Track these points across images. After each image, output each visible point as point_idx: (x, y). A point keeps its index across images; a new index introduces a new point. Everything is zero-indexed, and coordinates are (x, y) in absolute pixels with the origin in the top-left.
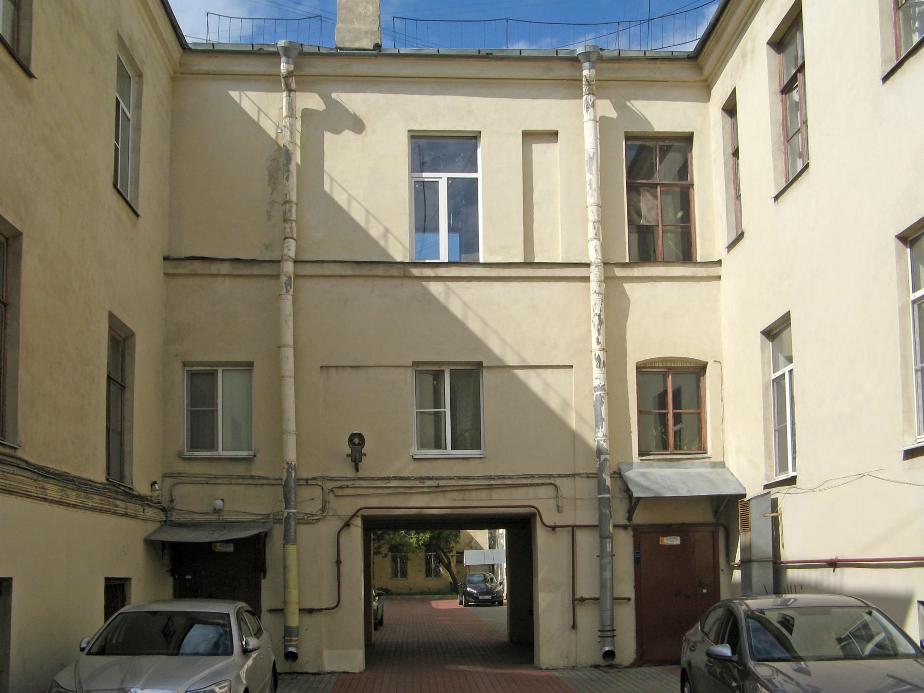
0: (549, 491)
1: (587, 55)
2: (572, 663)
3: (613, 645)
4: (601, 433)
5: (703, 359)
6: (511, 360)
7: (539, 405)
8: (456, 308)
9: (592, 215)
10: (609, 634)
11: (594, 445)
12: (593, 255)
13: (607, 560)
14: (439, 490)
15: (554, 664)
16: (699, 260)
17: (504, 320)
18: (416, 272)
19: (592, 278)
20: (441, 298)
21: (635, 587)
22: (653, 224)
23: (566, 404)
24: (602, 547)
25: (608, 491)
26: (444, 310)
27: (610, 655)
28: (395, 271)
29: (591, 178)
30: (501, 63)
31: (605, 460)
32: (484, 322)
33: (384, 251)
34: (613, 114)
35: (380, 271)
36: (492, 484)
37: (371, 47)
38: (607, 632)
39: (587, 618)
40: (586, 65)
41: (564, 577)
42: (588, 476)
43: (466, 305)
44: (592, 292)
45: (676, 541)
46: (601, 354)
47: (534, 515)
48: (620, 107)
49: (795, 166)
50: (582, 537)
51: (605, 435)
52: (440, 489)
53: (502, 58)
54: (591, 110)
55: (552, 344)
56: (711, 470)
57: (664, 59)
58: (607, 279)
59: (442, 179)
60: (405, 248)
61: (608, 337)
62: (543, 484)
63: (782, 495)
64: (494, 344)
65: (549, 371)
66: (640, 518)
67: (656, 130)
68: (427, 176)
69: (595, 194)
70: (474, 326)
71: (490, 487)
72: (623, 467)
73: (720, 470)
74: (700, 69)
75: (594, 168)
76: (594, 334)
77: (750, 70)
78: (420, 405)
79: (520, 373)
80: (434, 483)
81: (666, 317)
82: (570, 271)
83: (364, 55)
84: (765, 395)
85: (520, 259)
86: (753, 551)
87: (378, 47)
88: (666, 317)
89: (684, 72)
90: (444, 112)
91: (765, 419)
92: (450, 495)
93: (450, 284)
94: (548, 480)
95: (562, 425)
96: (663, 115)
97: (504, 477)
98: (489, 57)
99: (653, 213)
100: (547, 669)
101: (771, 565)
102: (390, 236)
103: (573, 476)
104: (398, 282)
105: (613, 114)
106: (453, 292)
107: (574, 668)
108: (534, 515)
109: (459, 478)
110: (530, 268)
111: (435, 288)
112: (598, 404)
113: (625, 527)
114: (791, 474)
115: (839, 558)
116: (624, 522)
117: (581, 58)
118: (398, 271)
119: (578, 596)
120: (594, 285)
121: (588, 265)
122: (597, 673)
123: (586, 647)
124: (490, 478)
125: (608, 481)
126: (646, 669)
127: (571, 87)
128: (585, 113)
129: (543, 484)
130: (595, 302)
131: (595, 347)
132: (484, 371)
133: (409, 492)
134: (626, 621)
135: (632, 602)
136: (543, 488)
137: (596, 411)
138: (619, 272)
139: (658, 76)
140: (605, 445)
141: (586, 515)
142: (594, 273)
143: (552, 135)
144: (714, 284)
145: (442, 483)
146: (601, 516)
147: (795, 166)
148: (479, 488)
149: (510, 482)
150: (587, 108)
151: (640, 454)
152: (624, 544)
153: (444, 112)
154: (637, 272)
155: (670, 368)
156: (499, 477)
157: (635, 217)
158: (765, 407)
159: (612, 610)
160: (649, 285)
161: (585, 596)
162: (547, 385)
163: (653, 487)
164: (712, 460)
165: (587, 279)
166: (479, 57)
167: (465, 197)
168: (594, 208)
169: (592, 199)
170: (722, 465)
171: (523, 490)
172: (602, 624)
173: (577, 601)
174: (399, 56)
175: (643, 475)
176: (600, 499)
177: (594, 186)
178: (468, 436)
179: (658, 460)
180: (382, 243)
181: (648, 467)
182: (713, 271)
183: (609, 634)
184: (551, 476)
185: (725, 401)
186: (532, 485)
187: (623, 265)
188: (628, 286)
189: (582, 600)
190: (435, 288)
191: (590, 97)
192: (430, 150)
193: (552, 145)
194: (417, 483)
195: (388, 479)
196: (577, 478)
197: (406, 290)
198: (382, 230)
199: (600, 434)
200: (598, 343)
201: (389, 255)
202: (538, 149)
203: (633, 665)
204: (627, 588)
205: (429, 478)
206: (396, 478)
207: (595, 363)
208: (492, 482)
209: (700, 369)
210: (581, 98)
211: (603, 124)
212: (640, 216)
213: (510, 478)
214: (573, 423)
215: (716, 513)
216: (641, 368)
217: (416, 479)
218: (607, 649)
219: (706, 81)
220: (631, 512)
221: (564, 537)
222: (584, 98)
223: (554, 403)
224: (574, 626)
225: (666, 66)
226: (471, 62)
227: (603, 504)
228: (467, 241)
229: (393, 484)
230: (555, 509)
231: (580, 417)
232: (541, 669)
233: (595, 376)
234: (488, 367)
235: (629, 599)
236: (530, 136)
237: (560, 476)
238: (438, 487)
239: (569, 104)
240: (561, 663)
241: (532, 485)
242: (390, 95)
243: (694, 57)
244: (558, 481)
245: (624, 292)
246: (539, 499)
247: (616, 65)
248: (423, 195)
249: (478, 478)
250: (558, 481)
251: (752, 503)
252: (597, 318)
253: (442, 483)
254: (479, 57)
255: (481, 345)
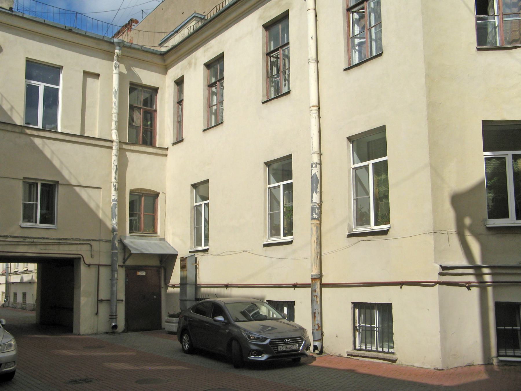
0: (87, 247)
1: (119, 44)
2: (95, 332)
3: (116, 322)
4: (115, 222)
5: (158, 191)
6: (73, 182)
7: (86, 205)
8: (48, 153)
9: (115, 118)
10: (115, 317)
11: (110, 227)
12: (114, 137)
13: (115, 282)
14: (33, 244)
15: (86, 332)
16: (157, 146)
17: (70, 162)
18: (28, 131)
19: (114, 148)
20: (40, 147)
21: (126, 295)
22: (139, 126)
23: (98, 206)
24: (113, 276)
25: (116, 249)
26: (41, 153)
27: (115, 327)
28: (17, 130)
29: (115, 100)
30: (76, 35)
31: (116, 234)
32: (61, 162)
33: (10, 118)
34: (125, 72)
35: (9, 128)
36: (61, 242)
37: (8, 9)
38: (113, 316)
39: (103, 309)
40: (118, 48)
41: (92, 289)
42: (106, 241)
43: (53, 152)
44: (113, 154)
45: (143, 273)
46: (116, 184)
47: (80, 258)
48: (128, 69)
49: (214, 118)
50: (103, 270)
51: (116, 223)
52: (34, 244)
53: (77, 34)
54: (117, 68)
55: (94, 177)
56: (159, 242)
57: (150, 52)
58: (121, 150)
59: (42, 86)
60: (21, 117)
61: (119, 176)
62: (85, 244)
63: (200, 257)
64: (66, 174)
65: (90, 189)
66: (129, 263)
67: (143, 83)
68: (34, 83)
69: (117, 108)
70: (56, 163)
71: (59, 244)
72: (122, 238)
73: (163, 242)
74: (164, 60)
75: (117, 96)
76: (113, 174)
77: (193, 72)
78: (24, 200)
79: (77, 189)
80: (32, 240)
81: (144, 170)
82: (103, 143)
83: (4, 12)
84: (191, 212)
85: (78, 133)
86: (188, 279)
87: (11, 9)
88: (144, 170)
89: (158, 60)
90: (46, 53)
91: (191, 222)
92: (39, 247)
93: (45, 140)
94: (88, 242)
95: (95, 215)
96: (147, 77)
97: (66, 239)
98: (70, 31)
99: (139, 121)
100: (83, 335)
101: (194, 286)
102: (14, 111)
103: (100, 240)
104: (17, 135)
105: (125, 72)
106: (46, 144)
107: (96, 334)
108: (80, 258)
109: (44, 238)
110: (82, 138)
111: (38, 141)
112: (114, 208)
113: (122, 266)
114: (204, 248)
115: (299, 283)
116: (122, 264)
117: (116, 44)
118: (20, 130)
119: (100, 299)
120: (114, 152)
121: (112, 141)
122: (108, 336)
123: (102, 323)
124: (60, 239)
125: (117, 243)
126: (130, 334)
127: (109, 56)
128: (114, 70)
129: (85, 244)
130: (114, 158)
131: (113, 180)
132: (59, 186)
133: (18, 244)
134: (121, 310)
135: (124, 302)
136: (85, 246)
137: (112, 211)
138: (125, 147)
139: (146, 59)
140: (116, 227)
141: (104, 260)
142: (115, 146)
143: (97, 76)
144: (164, 157)
145: (35, 240)
146: (113, 261)
147: (214, 118)
148: (54, 244)
149: (69, 242)
150: (116, 68)
151: (130, 233)
152: (121, 275)
153: (46, 53)
154: (132, 148)
155: (143, 194)
156: (64, 239)
157: (131, 121)
158: (191, 217)
159: (116, 306)
160: (137, 154)
161: (103, 299)
162: (90, 196)
163: (139, 248)
164: (160, 237)
165: (111, 148)
166: (64, 30)
167: (52, 98)
168: (116, 115)
169: (115, 110)
170: (164, 240)
171: (75, 246)
172: (111, 312)
173: (99, 301)
174: (23, 18)
175: (132, 242)
176: (113, 253)
177: (117, 104)
178: (48, 217)
179: (137, 236)
180: (9, 113)
181: (133, 238)
182: (164, 152)
183: (115, 317)
184: (89, 240)
185: (166, 211)
186: (80, 244)
187: (126, 144)
188: (128, 154)
189: (102, 301)
190: (38, 141)
191: (117, 63)
192: (34, 69)
193: (96, 80)
194: (22, 240)
195: (7, 237)
196: (101, 242)
197: (23, 139)
198: (9, 106)
199: (114, 222)
200: (115, 179)
201: (12, 120)
202: (89, 80)
203: (124, 332)
204: (122, 296)
205: (28, 238)
206: (11, 237)
207: (113, 188)
208: (61, 241)
209: (156, 195)
210: (113, 61)
211: (121, 74)
212: (133, 121)
213: (69, 240)
214: (101, 215)
215: (161, 261)
216: (132, 192)
217: (22, 237)
218: (114, 324)
219: (166, 66)
220: (125, 260)
221: (94, 270)
222: (115, 62)
223: (92, 205)
224: (97, 314)
225: (150, 56)
226: (62, 32)
227: (113, 255)
228: (51, 118)
229: (9, 239)
230: (90, 256)
231: (104, 212)
232: (79, 335)
233: (112, 194)
234: (61, 184)
235: (122, 300)
236: (87, 74)
237: (93, 240)
238: (33, 242)
239: (106, 63)
240: (90, 331)
241: (80, 244)
242: (17, 37)
243: (163, 55)
244: (92, 243)
245: (126, 156)
246: (82, 251)
247: (129, 50)
248: (31, 93)
249: (54, 239)
250: (92, 243)
251: (188, 258)
252: (115, 167)
253: (35, 240)
254: (64, 30)
255: (59, 173)
